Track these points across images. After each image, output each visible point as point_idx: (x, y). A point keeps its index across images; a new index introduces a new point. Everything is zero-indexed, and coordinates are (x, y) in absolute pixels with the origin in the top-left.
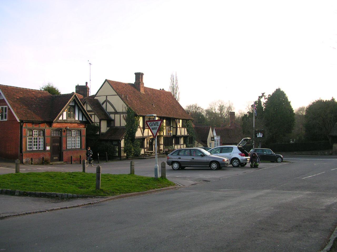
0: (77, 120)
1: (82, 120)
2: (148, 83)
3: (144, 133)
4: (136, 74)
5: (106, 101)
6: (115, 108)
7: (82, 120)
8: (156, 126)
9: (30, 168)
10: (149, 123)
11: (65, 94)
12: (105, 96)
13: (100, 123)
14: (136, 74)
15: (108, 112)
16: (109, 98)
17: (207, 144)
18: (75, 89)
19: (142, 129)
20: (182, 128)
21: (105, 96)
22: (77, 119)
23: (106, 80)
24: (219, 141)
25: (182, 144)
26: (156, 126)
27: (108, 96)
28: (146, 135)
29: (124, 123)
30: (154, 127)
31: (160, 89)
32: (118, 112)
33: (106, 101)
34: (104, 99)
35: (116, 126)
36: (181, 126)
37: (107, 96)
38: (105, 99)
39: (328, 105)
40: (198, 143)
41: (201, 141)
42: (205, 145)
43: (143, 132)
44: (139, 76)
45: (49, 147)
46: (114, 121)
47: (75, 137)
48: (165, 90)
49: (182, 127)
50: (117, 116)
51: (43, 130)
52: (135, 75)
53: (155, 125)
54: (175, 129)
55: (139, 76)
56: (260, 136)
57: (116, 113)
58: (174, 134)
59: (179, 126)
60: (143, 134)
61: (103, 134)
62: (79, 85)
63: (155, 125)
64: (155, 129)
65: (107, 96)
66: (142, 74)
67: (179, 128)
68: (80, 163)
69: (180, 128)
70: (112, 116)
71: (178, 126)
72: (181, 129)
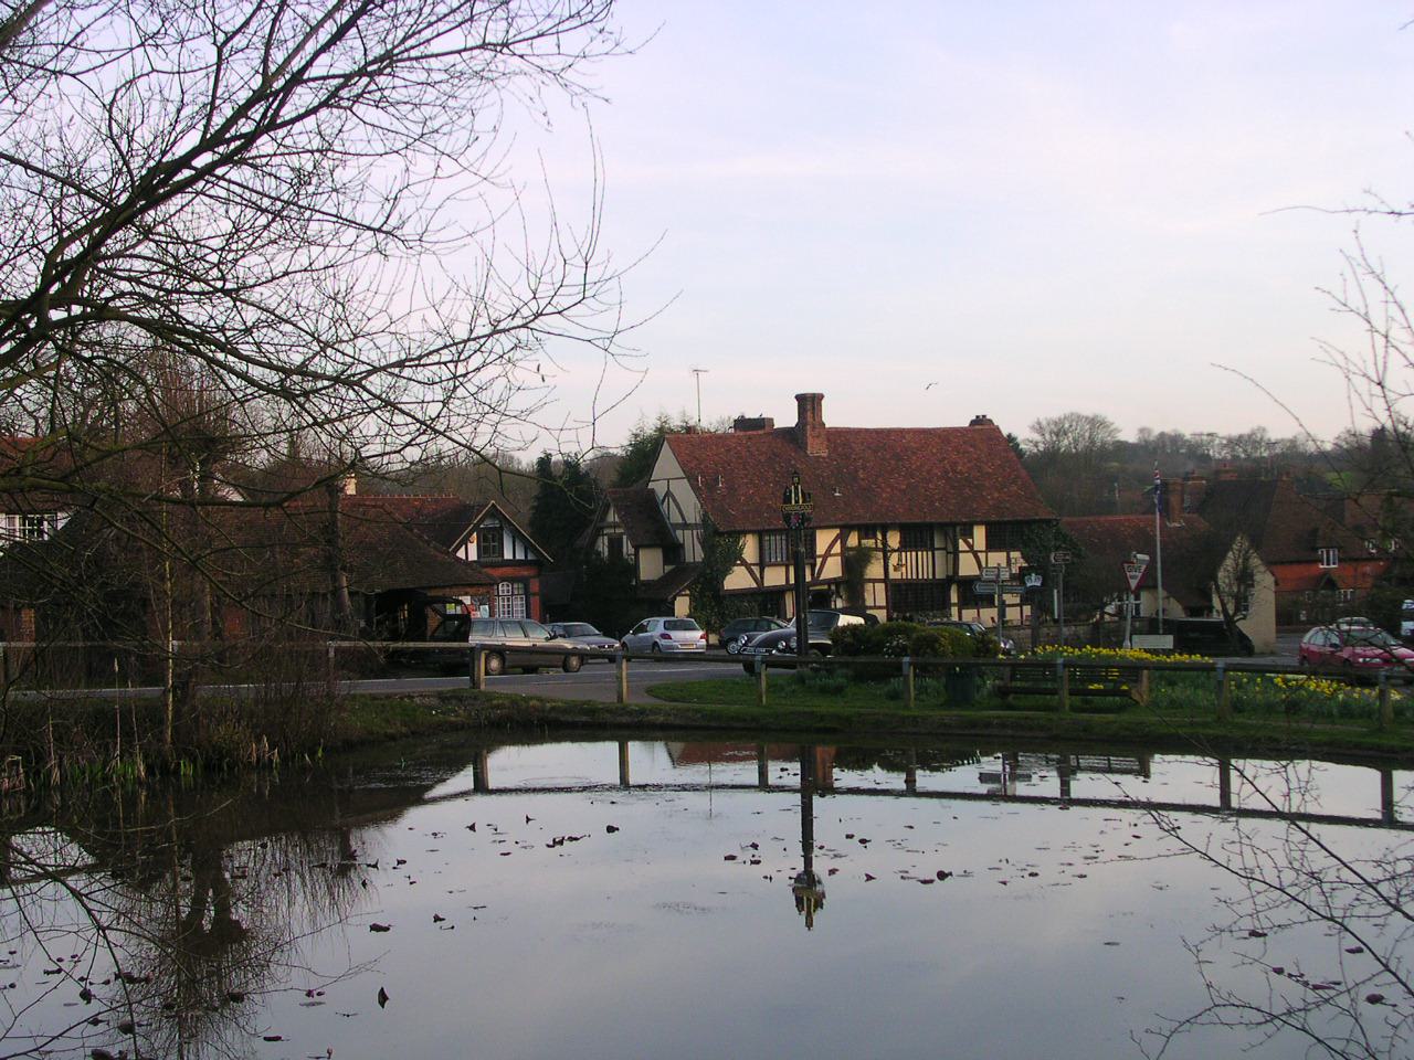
0: (474, 561)
1: (523, 558)
2: (834, 416)
4: (797, 397)
5: (669, 494)
7: (523, 558)
9: (606, 682)
13: (637, 554)
14: (797, 397)
15: (671, 524)
19: (756, 570)
22: (508, 555)
28: (835, 576)
29: (699, 556)
39: (1165, 484)
40: (1168, 598)
43: (758, 576)
50: (688, 533)
56: (1033, 584)
61: (648, 584)
62: (747, 417)
66: (821, 397)
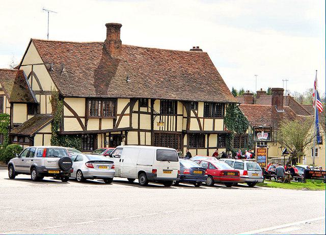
2: (127, 38)
4: (108, 25)
5: (32, 73)
14: (108, 25)
15: (33, 91)
18: (216, 67)
19: (83, 120)
20: (204, 118)
23: (31, 41)
24: (105, 164)
31: (194, 47)
44: (114, 29)
48: (201, 50)
50: (43, 97)
52: (105, 28)
55: (114, 29)
57: (42, 92)
58: (185, 129)
68: (208, 155)
69: (198, 119)
72: (201, 120)
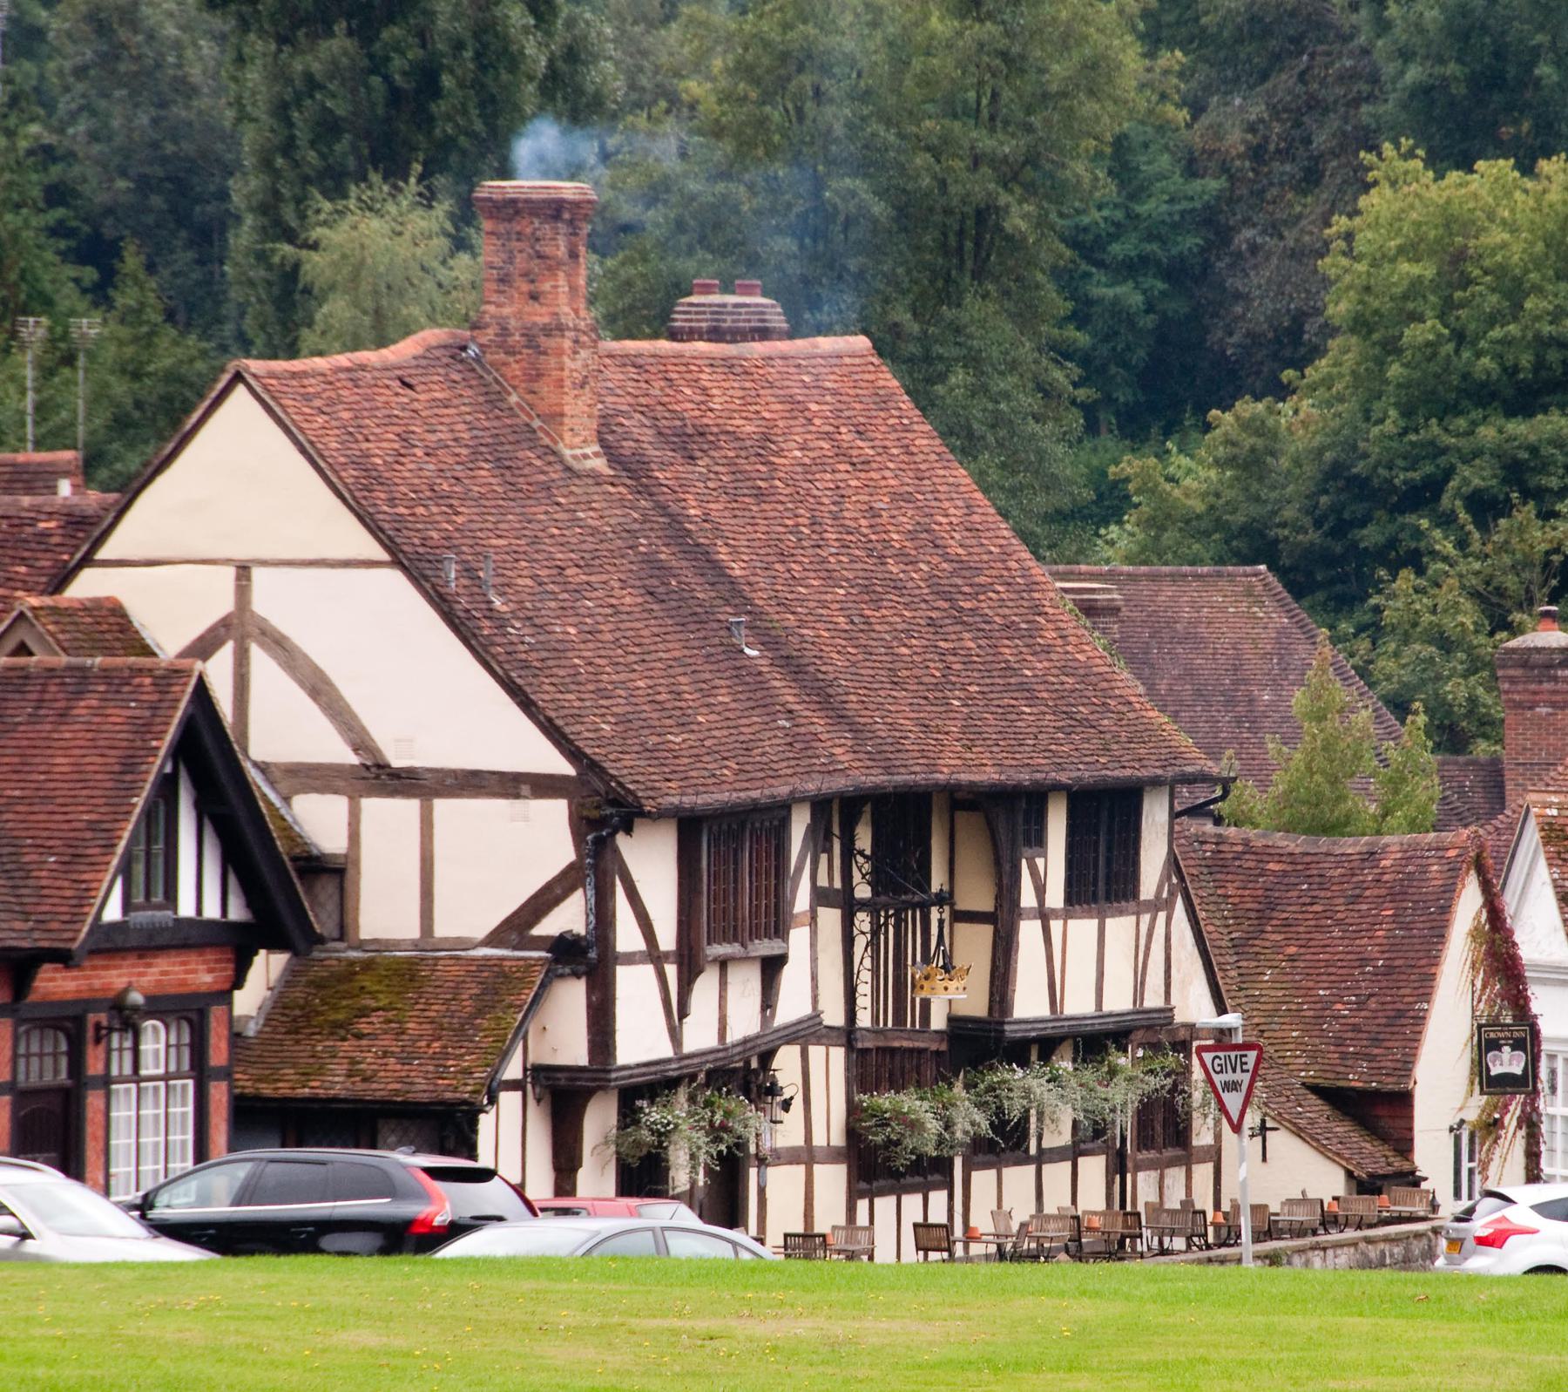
3: (683, 1013)
6: (354, 717)
8: (1238, 1076)
10: (1208, 1057)
11: (573, 833)
12: (227, 562)
16: (273, 598)
17: (1404, 1146)
19: (671, 970)
20: (1067, 915)
21: (227, 562)
22: (186, 908)
25: (1057, 1155)
26: (1238, 1076)
27: (257, 574)
30: (1229, 1076)
32: (396, 762)
33: (237, 629)
34: (213, 597)
35: (365, 934)
36: (1056, 896)
37: (243, 571)
38: (225, 605)
41: (1316, 1090)
42: (1375, 1157)
45: (1103, 1157)
46: (333, 873)
47: (156, 1089)
49: (1069, 899)
51: (68, 1025)
53: (1234, 1071)
54: (985, 932)
59: (1040, 890)
60: (675, 1035)
63: (1234, 1071)
64: (1232, 1086)
65: (243, 571)
67: (1037, 924)
69: (1044, 915)
70: (320, 821)
71: (1028, 898)
